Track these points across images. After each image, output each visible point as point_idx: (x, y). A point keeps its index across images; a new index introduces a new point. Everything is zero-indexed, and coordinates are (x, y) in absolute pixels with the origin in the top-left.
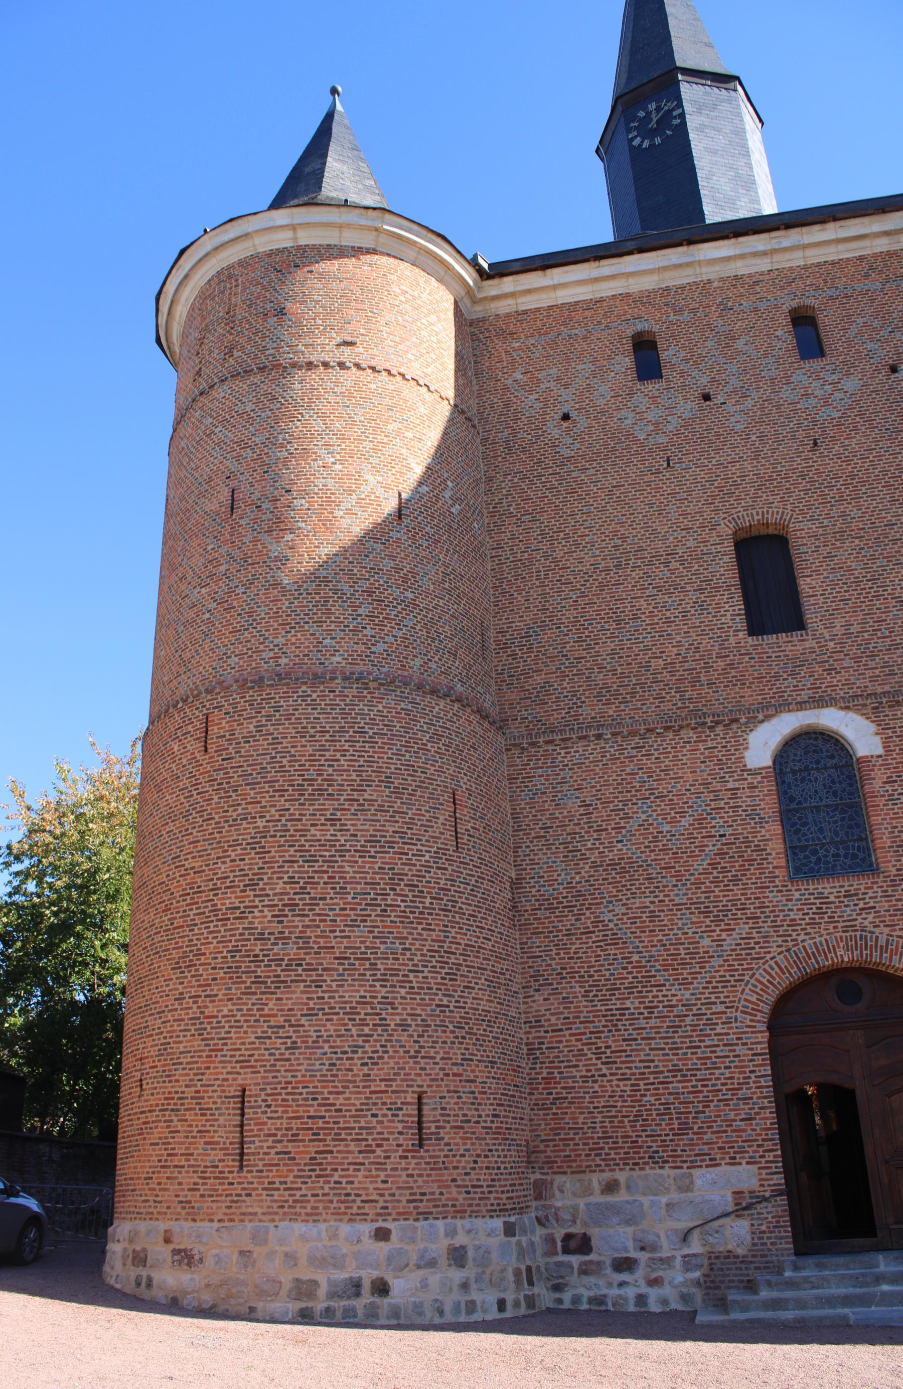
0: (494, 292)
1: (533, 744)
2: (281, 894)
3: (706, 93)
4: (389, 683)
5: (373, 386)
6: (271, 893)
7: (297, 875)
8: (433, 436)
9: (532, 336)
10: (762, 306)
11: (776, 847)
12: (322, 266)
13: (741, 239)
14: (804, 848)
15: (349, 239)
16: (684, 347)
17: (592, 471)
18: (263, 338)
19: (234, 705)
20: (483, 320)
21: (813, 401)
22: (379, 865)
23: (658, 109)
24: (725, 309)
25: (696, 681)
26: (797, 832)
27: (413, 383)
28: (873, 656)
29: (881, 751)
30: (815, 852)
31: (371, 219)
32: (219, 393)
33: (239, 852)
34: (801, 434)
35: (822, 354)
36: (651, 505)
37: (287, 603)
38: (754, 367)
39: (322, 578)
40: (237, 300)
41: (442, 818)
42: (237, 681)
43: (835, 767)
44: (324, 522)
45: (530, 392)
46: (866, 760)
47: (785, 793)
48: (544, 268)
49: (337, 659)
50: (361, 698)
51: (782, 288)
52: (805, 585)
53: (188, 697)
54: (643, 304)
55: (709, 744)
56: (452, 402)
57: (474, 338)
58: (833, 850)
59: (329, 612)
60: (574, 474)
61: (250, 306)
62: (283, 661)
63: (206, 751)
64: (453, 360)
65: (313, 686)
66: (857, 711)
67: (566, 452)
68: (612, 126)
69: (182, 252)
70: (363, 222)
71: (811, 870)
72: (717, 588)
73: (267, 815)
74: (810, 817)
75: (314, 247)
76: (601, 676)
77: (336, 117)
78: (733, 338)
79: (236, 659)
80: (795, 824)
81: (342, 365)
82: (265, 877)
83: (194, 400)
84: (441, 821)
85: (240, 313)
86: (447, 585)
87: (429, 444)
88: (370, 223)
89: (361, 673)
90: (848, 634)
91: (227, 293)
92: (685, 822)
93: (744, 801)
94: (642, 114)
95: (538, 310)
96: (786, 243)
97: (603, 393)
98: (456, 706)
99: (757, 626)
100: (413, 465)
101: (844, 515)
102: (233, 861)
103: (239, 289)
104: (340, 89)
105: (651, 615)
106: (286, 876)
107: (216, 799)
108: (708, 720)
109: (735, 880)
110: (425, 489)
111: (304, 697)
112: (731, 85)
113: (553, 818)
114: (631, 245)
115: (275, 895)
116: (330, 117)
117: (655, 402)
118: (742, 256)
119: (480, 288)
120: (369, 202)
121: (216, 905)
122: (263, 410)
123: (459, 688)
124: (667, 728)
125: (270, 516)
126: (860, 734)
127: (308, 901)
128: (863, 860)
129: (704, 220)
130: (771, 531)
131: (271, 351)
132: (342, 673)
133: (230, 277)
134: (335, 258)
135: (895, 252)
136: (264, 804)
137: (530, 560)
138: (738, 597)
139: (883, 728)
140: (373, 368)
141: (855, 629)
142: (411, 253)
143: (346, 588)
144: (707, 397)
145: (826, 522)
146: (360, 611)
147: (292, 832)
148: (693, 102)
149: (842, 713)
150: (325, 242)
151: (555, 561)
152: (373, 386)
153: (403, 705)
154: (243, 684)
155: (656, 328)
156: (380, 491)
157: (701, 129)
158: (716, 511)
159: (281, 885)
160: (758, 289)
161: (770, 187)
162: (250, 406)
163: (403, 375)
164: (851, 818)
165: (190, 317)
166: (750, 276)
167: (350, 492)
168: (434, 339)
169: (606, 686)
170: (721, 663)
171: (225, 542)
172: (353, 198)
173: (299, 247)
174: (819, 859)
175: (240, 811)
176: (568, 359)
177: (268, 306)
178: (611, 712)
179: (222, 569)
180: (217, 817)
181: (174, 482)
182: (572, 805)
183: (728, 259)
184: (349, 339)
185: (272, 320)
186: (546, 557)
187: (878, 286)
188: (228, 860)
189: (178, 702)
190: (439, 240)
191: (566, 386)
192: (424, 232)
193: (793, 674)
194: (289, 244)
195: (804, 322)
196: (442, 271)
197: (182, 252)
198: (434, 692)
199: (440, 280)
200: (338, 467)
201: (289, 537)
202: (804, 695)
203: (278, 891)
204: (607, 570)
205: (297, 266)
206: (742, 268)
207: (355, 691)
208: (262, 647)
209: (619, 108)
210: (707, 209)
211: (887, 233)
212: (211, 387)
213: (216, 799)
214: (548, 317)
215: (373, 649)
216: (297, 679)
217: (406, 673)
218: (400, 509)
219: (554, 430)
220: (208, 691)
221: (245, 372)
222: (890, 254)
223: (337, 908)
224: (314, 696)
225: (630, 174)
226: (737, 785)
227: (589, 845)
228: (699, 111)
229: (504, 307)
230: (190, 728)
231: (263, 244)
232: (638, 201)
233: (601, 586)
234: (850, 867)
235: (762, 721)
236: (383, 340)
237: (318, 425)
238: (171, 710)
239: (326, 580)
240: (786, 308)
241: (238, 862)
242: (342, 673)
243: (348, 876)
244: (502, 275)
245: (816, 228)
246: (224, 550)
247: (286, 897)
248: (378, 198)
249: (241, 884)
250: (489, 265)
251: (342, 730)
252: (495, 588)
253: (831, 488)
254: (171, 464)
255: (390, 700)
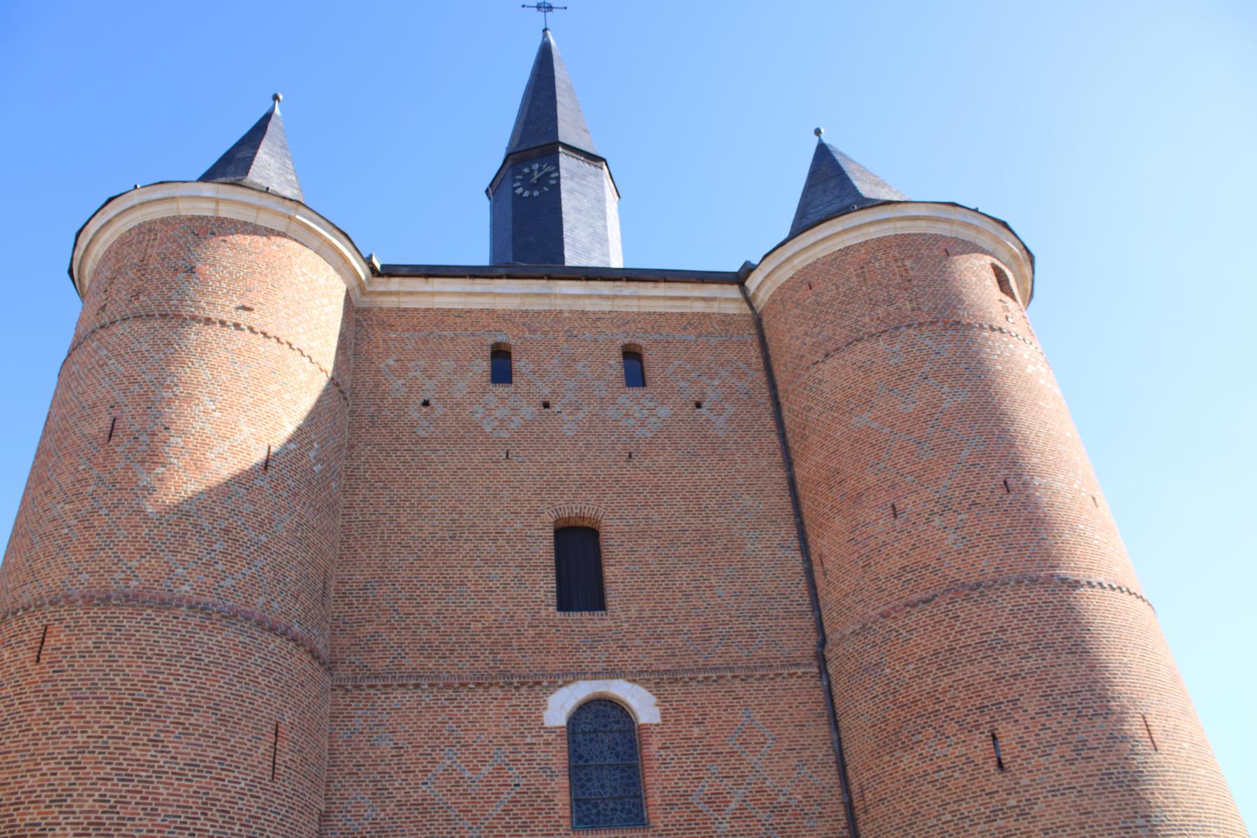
0: (381, 288)
1: (357, 687)
2: (89, 812)
3: (579, 166)
4: (231, 616)
5: (262, 349)
6: (77, 810)
7: (108, 794)
8: (307, 402)
9: (408, 330)
10: (601, 338)
11: (562, 800)
12: (236, 238)
13: (591, 283)
14: (586, 801)
15: (264, 220)
16: (533, 361)
17: (442, 453)
18: (170, 289)
19: (76, 620)
20: (368, 310)
21: (632, 421)
22: (195, 789)
23: (540, 170)
24: (570, 335)
25: (508, 645)
26: (582, 786)
27: (298, 353)
28: (659, 638)
29: (658, 720)
30: (596, 806)
31: (287, 208)
32: (119, 329)
33: (53, 765)
34: (619, 447)
35: (644, 385)
36: (488, 489)
37: (147, 531)
38: (588, 387)
39: (183, 512)
40: (152, 251)
41: (262, 748)
42: (83, 597)
43: (620, 731)
44: (195, 462)
45: (399, 377)
46: (646, 727)
47: (575, 751)
48: (428, 276)
49: (186, 588)
50: (203, 627)
51: (618, 327)
52: (610, 572)
53: (30, 606)
54: (505, 320)
55: (514, 702)
56: (330, 375)
57: (358, 323)
58: (611, 805)
59: (185, 544)
60: (426, 453)
61: (163, 259)
62: (134, 583)
63: (38, 661)
64: (336, 339)
65: (159, 610)
66: (641, 684)
67: (423, 434)
68: (502, 174)
69: (110, 200)
70: (279, 209)
71: (592, 822)
72: (535, 567)
73: (90, 731)
74: (595, 774)
75: (232, 221)
76: (426, 632)
77: (273, 118)
78: (574, 360)
79: (87, 576)
80: (580, 780)
81: (237, 326)
82: (75, 794)
83: (93, 332)
84: (261, 750)
85: (153, 264)
86: (299, 534)
87: (303, 407)
88: (284, 211)
89: (207, 604)
90: (640, 618)
91: (145, 244)
92: (485, 770)
93: (539, 756)
94: (526, 170)
95: (416, 310)
96: (626, 292)
97: (461, 388)
98: (291, 644)
99: (565, 603)
100: (286, 424)
101: (647, 518)
102: (45, 774)
103: (157, 243)
104: (281, 97)
105: (476, 584)
106: (97, 794)
107: (38, 710)
108: (515, 681)
109: (525, 826)
110: (293, 446)
111: (147, 621)
112: (599, 164)
113: (366, 756)
114: (501, 271)
115: (82, 812)
116: (268, 117)
117: (503, 402)
118: (590, 296)
119: (370, 283)
120: (288, 193)
121: (14, 820)
122: (157, 352)
123: (296, 628)
124: (478, 685)
125: (146, 448)
126: (643, 705)
127: (115, 821)
128: (637, 815)
129: (563, 262)
130: (586, 524)
131: (175, 302)
132: (189, 601)
133: (150, 230)
134: (249, 234)
135: (708, 315)
136: (88, 719)
137: (377, 522)
138: (552, 576)
139: (662, 700)
140: (265, 334)
141: (647, 614)
142: (317, 243)
143: (206, 524)
144: (546, 405)
145: (632, 522)
146: (215, 547)
147: (112, 750)
148: (568, 171)
149: (629, 685)
150: (242, 218)
151: (399, 526)
152: (262, 349)
153: (241, 638)
154: (89, 600)
155: (512, 342)
156: (252, 442)
157: (571, 191)
158: (543, 501)
159: (90, 802)
160: (599, 324)
161: (619, 247)
162: (145, 347)
163: (290, 345)
164: (629, 777)
165: (106, 257)
166: (594, 313)
167: (224, 438)
168: (323, 318)
169: (429, 642)
170: (531, 632)
171: (97, 465)
172: (274, 187)
173: (218, 219)
174: (599, 813)
175: (62, 724)
176: (435, 356)
177: (180, 263)
178: (430, 665)
179: (90, 489)
180: (35, 728)
181: (59, 401)
182: (386, 746)
183: (579, 296)
184: (248, 305)
185: (181, 276)
186: (391, 521)
187: (693, 338)
188: (38, 773)
189: (18, 610)
190: (342, 237)
191: (430, 377)
192: (330, 228)
193: (592, 648)
194: (210, 214)
195: (632, 356)
196: (340, 262)
197: (110, 200)
198: (272, 629)
199: (338, 270)
200: (217, 414)
201: (160, 470)
202: (600, 667)
203: (86, 808)
204: (443, 539)
205: (213, 234)
206: (588, 305)
207: (198, 620)
208: (114, 568)
209: (510, 163)
210: (568, 253)
211: (704, 299)
212: (113, 323)
213: (38, 710)
214: (425, 317)
215: (222, 583)
216: (144, 602)
217: (248, 609)
218: (267, 461)
219: (415, 412)
220: (52, 603)
221: (148, 315)
222: (705, 315)
223: (145, 829)
224: (158, 620)
225: (510, 215)
226: (534, 740)
227: (397, 785)
228: (572, 178)
229: (389, 302)
230: (26, 637)
231: (186, 209)
232: (513, 237)
233: (436, 553)
234: (625, 820)
235: (561, 686)
236: (278, 311)
237: (205, 375)
238: (9, 617)
239: (188, 514)
240: (619, 343)
241: (49, 777)
242: (189, 601)
243: (161, 798)
244: (390, 275)
245: (650, 285)
246: (95, 472)
247: (93, 816)
248: (296, 192)
249: (48, 800)
250: (382, 266)
251: (180, 655)
252: (342, 542)
253: (639, 494)
254: (59, 385)
255: (230, 632)
